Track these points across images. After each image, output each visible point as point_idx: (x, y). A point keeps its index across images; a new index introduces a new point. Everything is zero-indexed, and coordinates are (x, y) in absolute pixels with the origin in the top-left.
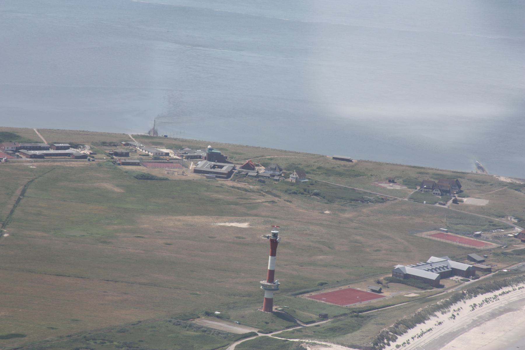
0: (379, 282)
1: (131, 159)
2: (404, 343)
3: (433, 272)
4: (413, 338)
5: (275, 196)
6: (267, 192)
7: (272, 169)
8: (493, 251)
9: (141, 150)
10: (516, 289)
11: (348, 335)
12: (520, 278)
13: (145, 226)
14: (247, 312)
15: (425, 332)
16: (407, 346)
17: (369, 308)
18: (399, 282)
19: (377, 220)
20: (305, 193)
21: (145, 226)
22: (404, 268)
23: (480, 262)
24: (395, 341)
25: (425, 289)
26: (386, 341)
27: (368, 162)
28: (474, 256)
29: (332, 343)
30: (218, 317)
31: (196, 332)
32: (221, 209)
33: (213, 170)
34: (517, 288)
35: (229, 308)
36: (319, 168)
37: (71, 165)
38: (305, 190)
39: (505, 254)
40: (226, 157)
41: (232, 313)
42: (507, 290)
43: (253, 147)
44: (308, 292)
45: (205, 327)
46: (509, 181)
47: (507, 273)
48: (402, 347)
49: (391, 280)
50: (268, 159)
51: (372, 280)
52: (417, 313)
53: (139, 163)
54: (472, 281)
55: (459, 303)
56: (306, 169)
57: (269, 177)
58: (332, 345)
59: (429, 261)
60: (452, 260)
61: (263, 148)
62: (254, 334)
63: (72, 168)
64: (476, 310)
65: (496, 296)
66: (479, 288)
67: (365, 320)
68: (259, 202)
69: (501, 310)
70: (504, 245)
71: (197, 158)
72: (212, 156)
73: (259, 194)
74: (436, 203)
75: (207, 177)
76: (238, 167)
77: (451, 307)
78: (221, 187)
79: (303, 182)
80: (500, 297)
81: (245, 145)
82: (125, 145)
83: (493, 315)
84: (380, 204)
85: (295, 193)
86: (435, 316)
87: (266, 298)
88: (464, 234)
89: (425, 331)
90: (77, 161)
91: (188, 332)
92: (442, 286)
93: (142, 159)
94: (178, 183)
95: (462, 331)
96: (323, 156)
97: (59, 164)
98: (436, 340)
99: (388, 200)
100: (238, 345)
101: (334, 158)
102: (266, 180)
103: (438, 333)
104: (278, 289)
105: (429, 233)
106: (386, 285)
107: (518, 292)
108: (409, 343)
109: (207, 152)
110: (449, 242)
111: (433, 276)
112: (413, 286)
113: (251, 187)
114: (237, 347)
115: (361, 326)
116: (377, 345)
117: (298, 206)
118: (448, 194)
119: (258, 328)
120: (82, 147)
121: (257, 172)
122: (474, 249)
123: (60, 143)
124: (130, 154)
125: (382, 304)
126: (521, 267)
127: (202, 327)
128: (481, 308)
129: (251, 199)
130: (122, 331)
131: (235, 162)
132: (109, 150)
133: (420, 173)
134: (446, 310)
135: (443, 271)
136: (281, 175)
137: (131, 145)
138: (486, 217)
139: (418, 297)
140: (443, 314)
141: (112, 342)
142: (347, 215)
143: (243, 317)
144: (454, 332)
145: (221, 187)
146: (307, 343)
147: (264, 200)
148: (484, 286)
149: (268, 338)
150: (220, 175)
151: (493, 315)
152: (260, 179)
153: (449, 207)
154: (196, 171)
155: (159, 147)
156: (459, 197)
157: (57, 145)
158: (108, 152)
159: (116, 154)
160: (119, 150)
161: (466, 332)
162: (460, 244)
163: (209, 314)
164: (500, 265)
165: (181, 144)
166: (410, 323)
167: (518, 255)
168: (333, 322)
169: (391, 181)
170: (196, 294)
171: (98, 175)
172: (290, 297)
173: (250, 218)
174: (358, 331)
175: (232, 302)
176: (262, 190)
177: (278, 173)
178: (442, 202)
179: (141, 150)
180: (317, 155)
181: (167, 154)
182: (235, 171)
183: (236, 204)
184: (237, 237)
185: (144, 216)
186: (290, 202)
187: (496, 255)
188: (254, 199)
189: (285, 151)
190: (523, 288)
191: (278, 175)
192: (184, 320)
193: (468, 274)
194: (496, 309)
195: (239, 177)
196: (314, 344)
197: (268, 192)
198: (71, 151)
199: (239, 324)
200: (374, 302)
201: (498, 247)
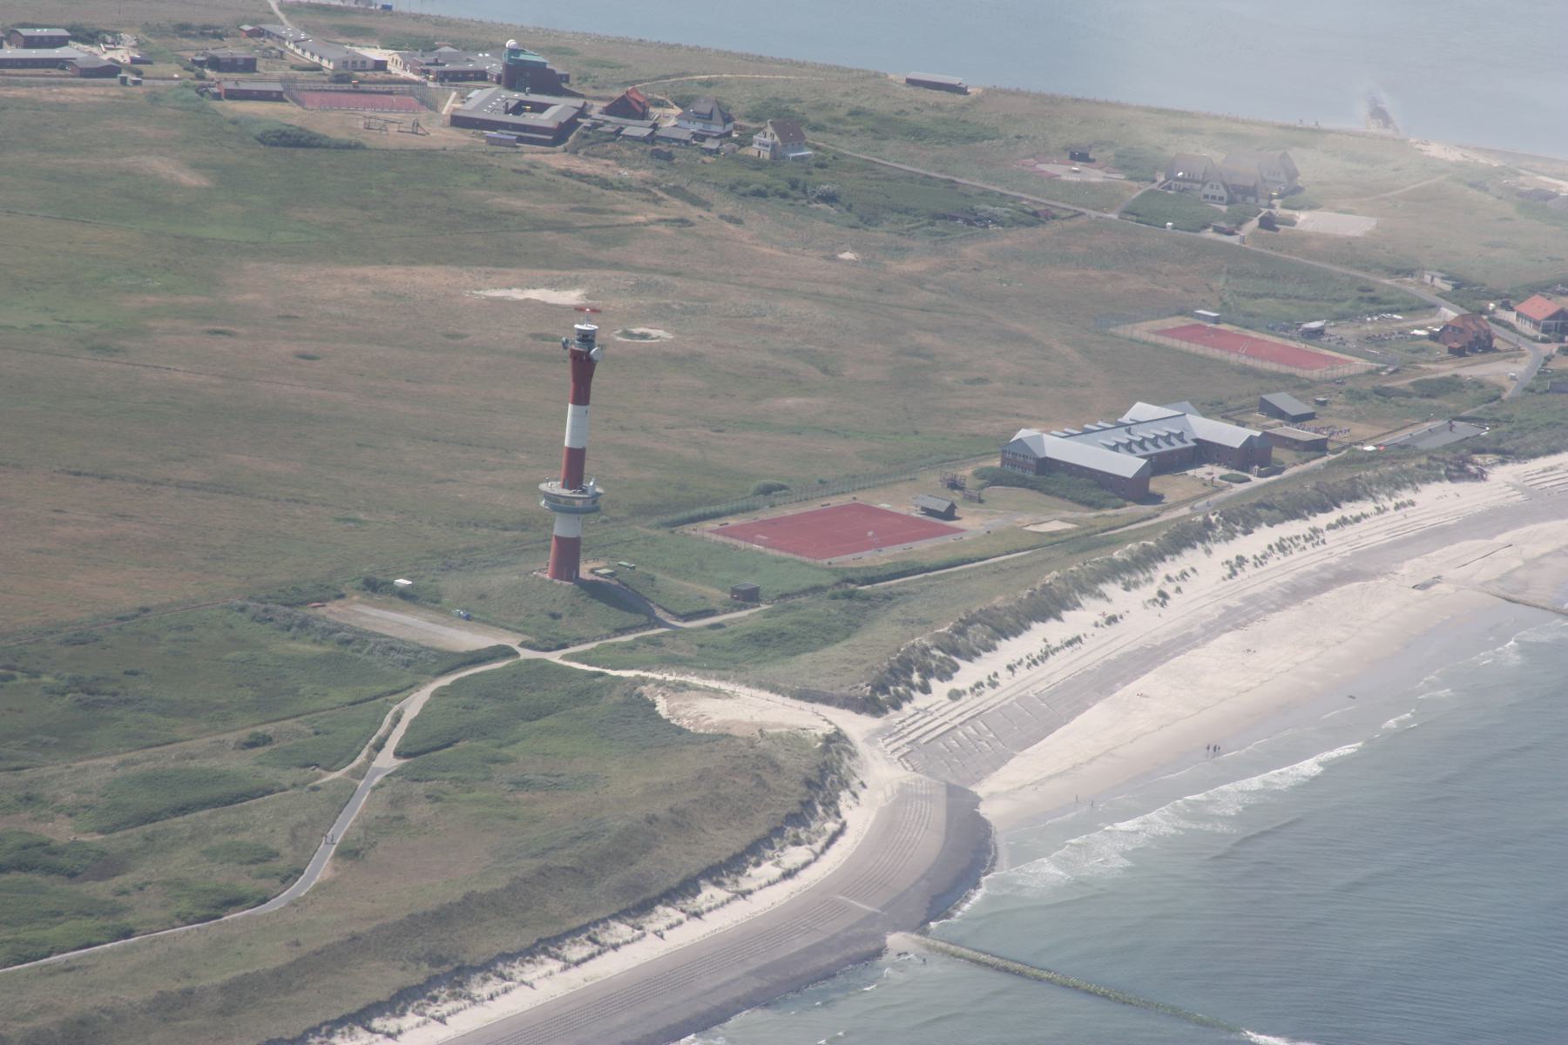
0: (954, 485)
1: (261, 80)
2: (979, 685)
3: (1131, 451)
4: (1011, 668)
5: (695, 201)
6: (668, 191)
7: (699, 116)
8: (1350, 385)
9: (299, 51)
10: (1386, 509)
11: (803, 656)
12: (1405, 472)
13: (249, 297)
14: (499, 580)
15: (1057, 649)
16: (989, 692)
17: (901, 569)
18: (1022, 483)
19: (1001, 281)
20: (792, 193)
21: (249, 297)
22: (1039, 439)
23: (1298, 420)
24: (950, 677)
25: (1100, 507)
26: (916, 678)
27: (1017, 93)
28: (1282, 400)
29: (741, 682)
30: (404, 594)
31: (321, 644)
32: (506, 243)
33: (511, 118)
34: (1390, 504)
35: (448, 568)
36: (856, 113)
37: (62, 98)
38: (794, 185)
39: (1384, 394)
40: (566, 78)
41: (452, 584)
42: (1356, 513)
43: (660, 45)
44: (717, 515)
45: (352, 629)
46: (1455, 156)
47: (1372, 457)
48: (969, 696)
49: (995, 479)
50: (701, 83)
51: (934, 478)
52: (1038, 587)
53: (280, 93)
54: (1256, 481)
55: (1187, 553)
56: (813, 118)
57: (687, 142)
58: (743, 691)
59: (1126, 419)
60: (1206, 415)
61: (690, 49)
62: (505, 652)
63: (62, 107)
64: (1241, 575)
65: (1315, 531)
66: (1261, 505)
67: (874, 607)
68: (638, 224)
69: (1327, 575)
70: (1390, 364)
71: (470, 79)
72: (519, 75)
73: (644, 196)
74: (1205, 227)
75: (492, 142)
76: (596, 110)
77: (1160, 566)
78: (527, 172)
79: (794, 159)
80: (1330, 536)
81: (635, 37)
82: (251, 34)
83: (1296, 593)
84: (1024, 231)
85: (759, 194)
86: (1101, 595)
87: (558, 538)
88: (1271, 330)
89: (1055, 643)
90: (82, 85)
91: (293, 645)
92: (1156, 499)
93: (293, 80)
94: (394, 157)
95: (1185, 642)
96: (876, 75)
97: (22, 92)
98: (1089, 673)
99: (1054, 217)
100: (442, 688)
101: (910, 82)
102: (675, 152)
103: (1101, 647)
104: (596, 510)
105: (1158, 324)
106: (974, 493)
107: (1394, 518)
108: (993, 685)
109: (505, 59)
110: (1216, 353)
111: (1128, 465)
112: (1064, 497)
113: (625, 173)
114: (440, 694)
115: (858, 626)
116: (885, 690)
117: (762, 238)
118: (1251, 200)
119: (525, 632)
120: (109, 39)
121: (655, 126)
122: (1291, 376)
123: (34, 26)
124: (261, 64)
125: (949, 556)
126: (1421, 437)
127: (339, 628)
128: (1261, 569)
129: (613, 212)
130: (80, 639)
131: (593, 93)
132: (194, 49)
133: (1175, 131)
134: (1141, 577)
135: (1166, 448)
136: (729, 134)
137: (269, 35)
138: (1354, 272)
139: (1069, 531)
140: (1127, 589)
141: (37, 675)
142: (910, 266)
143: (483, 597)
144: (1155, 648)
145: (527, 172)
146: (660, 684)
147: (653, 216)
148: (1281, 498)
149: (545, 667)
150: (530, 135)
151: (1296, 593)
152: (657, 148)
153: (1243, 240)
154: (458, 121)
155: (361, 41)
156: (1285, 207)
157: (25, 32)
158: (190, 56)
159: (215, 64)
160: (229, 49)
161: (1196, 646)
162: (1250, 362)
163: (374, 587)
164: (1360, 430)
165: (430, 31)
166: (1010, 620)
167: (1428, 396)
168: (769, 615)
169: (1080, 156)
170: (354, 520)
171: (140, 129)
172: (654, 533)
173: (597, 273)
174: (838, 646)
175: (461, 546)
176: (656, 184)
177: (718, 129)
178: (1223, 225)
179: (299, 51)
180: (858, 71)
181: (381, 66)
182: (586, 122)
183: (562, 228)
184: (535, 336)
185: (253, 265)
186: (738, 222)
187: (1356, 396)
188: (624, 213)
189: (760, 59)
190: (1412, 504)
191: (720, 136)
192: (291, 604)
193: (1250, 457)
194: (1309, 574)
195: (597, 140)
196: (681, 687)
197: (676, 192)
198: (74, 51)
199: (468, 618)
200: (923, 549)
201: (1370, 372)
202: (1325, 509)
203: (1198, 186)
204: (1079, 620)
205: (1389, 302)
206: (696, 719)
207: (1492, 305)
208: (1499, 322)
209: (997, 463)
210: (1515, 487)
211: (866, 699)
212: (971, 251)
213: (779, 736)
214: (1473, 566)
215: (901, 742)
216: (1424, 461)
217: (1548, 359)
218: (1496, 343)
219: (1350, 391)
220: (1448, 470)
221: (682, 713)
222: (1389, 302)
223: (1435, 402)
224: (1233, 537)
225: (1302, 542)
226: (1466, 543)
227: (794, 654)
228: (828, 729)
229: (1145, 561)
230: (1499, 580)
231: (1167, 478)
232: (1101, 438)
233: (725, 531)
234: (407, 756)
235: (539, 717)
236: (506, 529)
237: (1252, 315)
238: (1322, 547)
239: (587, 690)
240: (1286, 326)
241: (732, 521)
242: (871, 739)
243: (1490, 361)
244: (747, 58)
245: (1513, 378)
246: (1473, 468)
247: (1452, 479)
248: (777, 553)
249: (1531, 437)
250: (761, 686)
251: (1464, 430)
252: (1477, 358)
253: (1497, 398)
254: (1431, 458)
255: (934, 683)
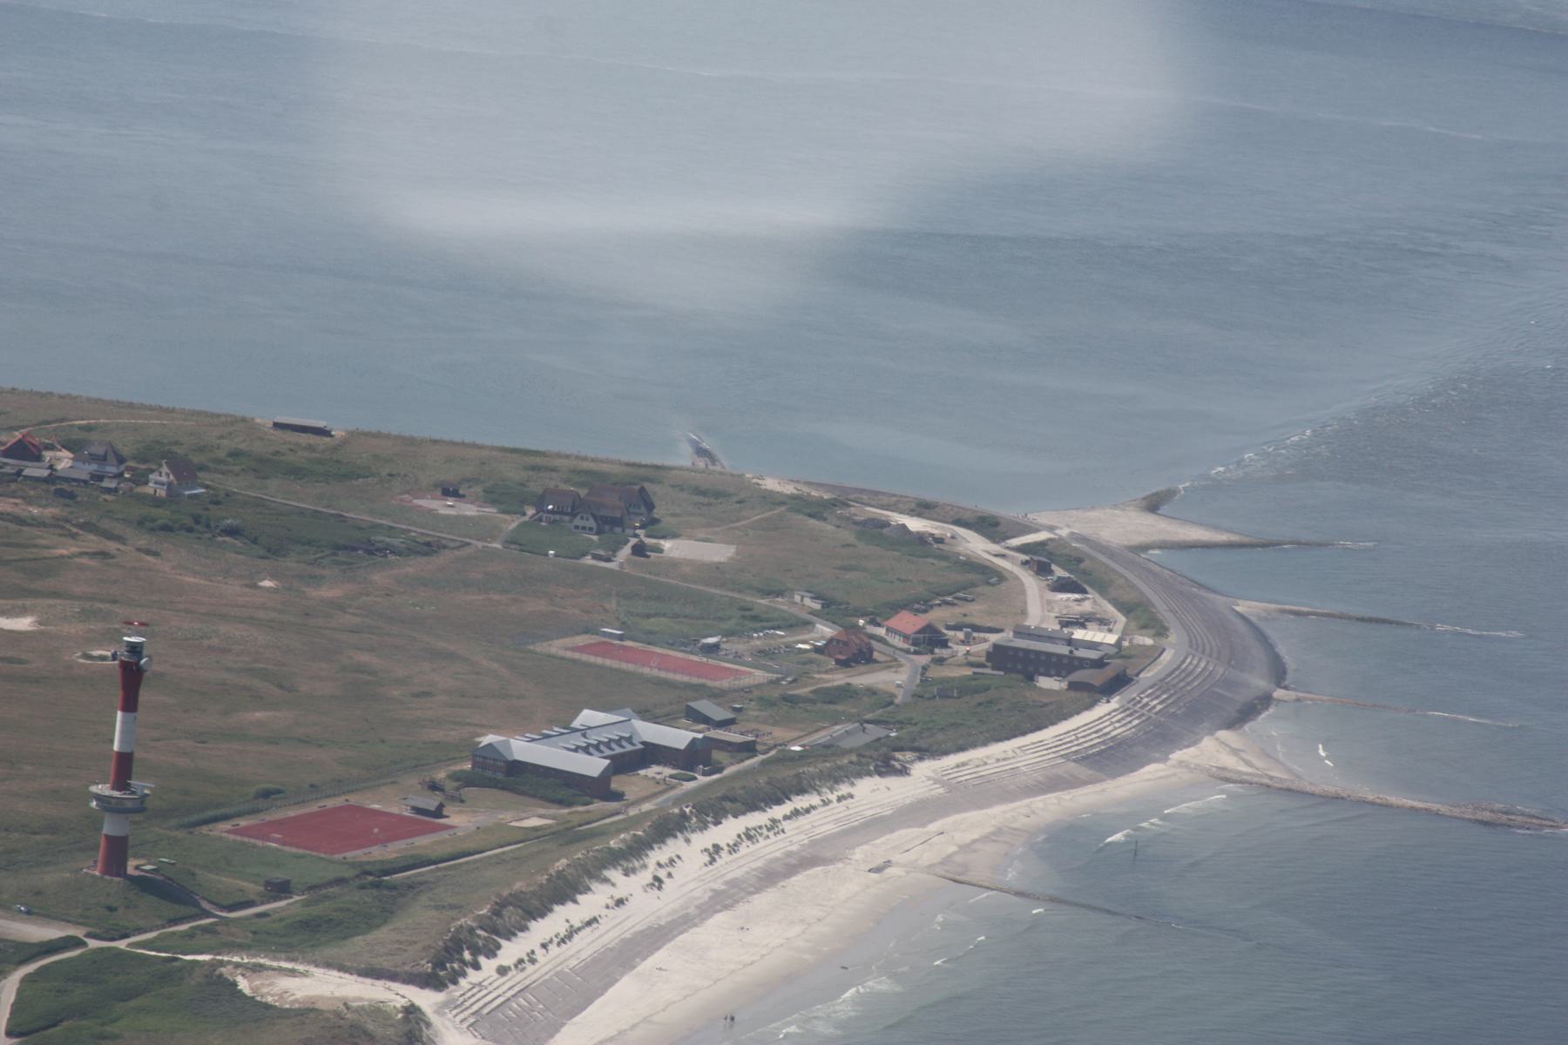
0: (434, 787)
2: (521, 961)
4: (544, 946)
6: (82, 526)
7: (94, 458)
10: (830, 802)
12: (840, 768)
14: (50, 877)
15: (579, 929)
16: (530, 968)
19: (414, 605)
20: (198, 527)
22: (507, 743)
25: (570, 805)
28: (704, 706)
29: (309, 963)
34: (833, 797)
36: (235, 454)
39: (791, 700)
42: (806, 805)
43: (33, 393)
47: (800, 757)
50: (81, 428)
51: (413, 781)
55: (670, 842)
57: (85, 482)
59: (576, 724)
61: (61, 397)
65: (774, 821)
66: (725, 798)
68: (62, 556)
69: (793, 861)
73: (59, 531)
74: (584, 555)
77: (651, 853)
79: (190, 496)
80: (786, 825)
83: (770, 876)
85: (166, 528)
86: (606, 880)
87: (107, 837)
88: (671, 645)
89: (577, 924)
92: (618, 796)
96: (244, 420)
99: (445, 547)
105: (568, 641)
108: (533, 961)
110: (631, 667)
111: (593, 766)
112: (534, 796)
114: (26, 980)
115: (392, 913)
121: (51, 467)
122: (703, 686)
128: (735, 856)
129: (35, 546)
133: (534, 468)
134: (637, 864)
136: (121, 474)
139: (550, 826)
140: (626, 875)
142: (327, 592)
143: (38, 893)
144: (661, 928)
146: (237, 965)
147: (75, 550)
151: (770, 876)
161: (696, 925)
162: (663, 674)
164: (780, 733)
166: (536, 903)
169: (449, 491)
176: (67, 521)
177: (112, 470)
178: (602, 552)
186: (156, 554)
187: (766, 703)
189: (131, 406)
190: (851, 796)
193: (691, 759)
194: (777, 859)
196: (258, 969)
197: (87, 527)
199: (28, 913)
200: (423, 843)
201: (771, 682)
202: (779, 802)
203: (567, 518)
204: (592, 901)
205: (768, 620)
206: (281, 996)
207: (861, 622)
208: (873, 637)
209: (468, 766)
210: (936, 782)
211: (429, 975)
212: (378, 578)
213: (362, 1008)
214: (918, 850)
215: (466, 1013)
216: (854, 758)
217: (925, 668)
218: (876, 655)
219: (761, 699)
220: (876, 767)
221: (265, 990)
222: (768, 620)
223: (839, 708)
224: (706, 827)
225: (765, 831)
226: (903, 832)
227: (345, 938)
228: (404, 1002)
229: (635, 851)
230: (942, 863)
231: (623, 777)
232: (561, 741)
233: (237, 831)
234: (18, 1036)
235: (130, 998)
236: (35, 833)
237: (651, 632)
238: (782, 836)
239: (170, 974)
240: (687, 642)
241: (243, 823)
242: (440, 1009)
243: (873, 671)
244: (118, 405)
245: (899, 686)
246: (897, 765)
247: (881, 774)
248: (294, 850)
249: (940, 736)
250: (328, 965)
251: (875, 732)
252: (862, 668)
253: (891, 703)
254: (860, 755)
255: (482, 960)
